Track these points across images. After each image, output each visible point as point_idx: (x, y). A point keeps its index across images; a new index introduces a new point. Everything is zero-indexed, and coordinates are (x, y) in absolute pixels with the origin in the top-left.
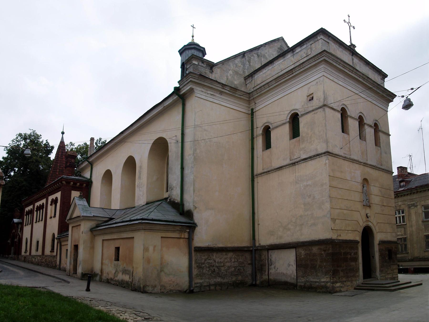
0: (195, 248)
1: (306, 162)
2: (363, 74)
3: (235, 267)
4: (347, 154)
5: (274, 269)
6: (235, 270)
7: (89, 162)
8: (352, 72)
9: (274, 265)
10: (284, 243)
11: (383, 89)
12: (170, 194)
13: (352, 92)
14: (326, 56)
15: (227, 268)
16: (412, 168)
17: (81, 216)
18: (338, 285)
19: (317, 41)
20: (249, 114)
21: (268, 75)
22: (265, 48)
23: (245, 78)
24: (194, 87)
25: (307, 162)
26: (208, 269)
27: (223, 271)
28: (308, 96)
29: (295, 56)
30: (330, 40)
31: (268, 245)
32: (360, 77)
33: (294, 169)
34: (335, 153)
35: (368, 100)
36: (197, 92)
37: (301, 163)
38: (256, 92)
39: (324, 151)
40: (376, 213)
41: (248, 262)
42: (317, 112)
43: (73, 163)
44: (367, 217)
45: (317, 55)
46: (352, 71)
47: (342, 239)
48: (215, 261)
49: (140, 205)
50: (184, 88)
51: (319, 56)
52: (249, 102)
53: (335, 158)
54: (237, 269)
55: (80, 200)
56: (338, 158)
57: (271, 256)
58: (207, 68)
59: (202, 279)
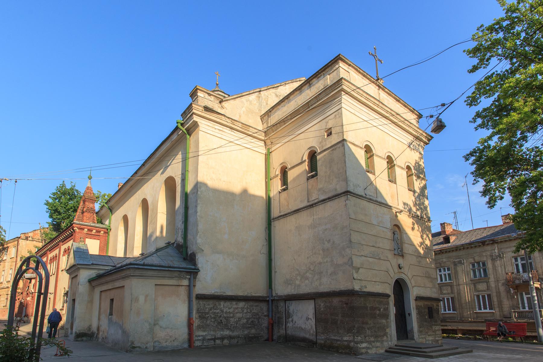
1: (324, 203)
3: (248, 318)
6: (247, 322)
9: (291, 318)
16: (457, 226)
18: (364, 345)
26: (213, 320)
36: (202, 126)
37: (319, 205)
39: (344, 190)
41: (263, 313)
48: (222, 311)
57: (288, 307)
59: (204, 331)
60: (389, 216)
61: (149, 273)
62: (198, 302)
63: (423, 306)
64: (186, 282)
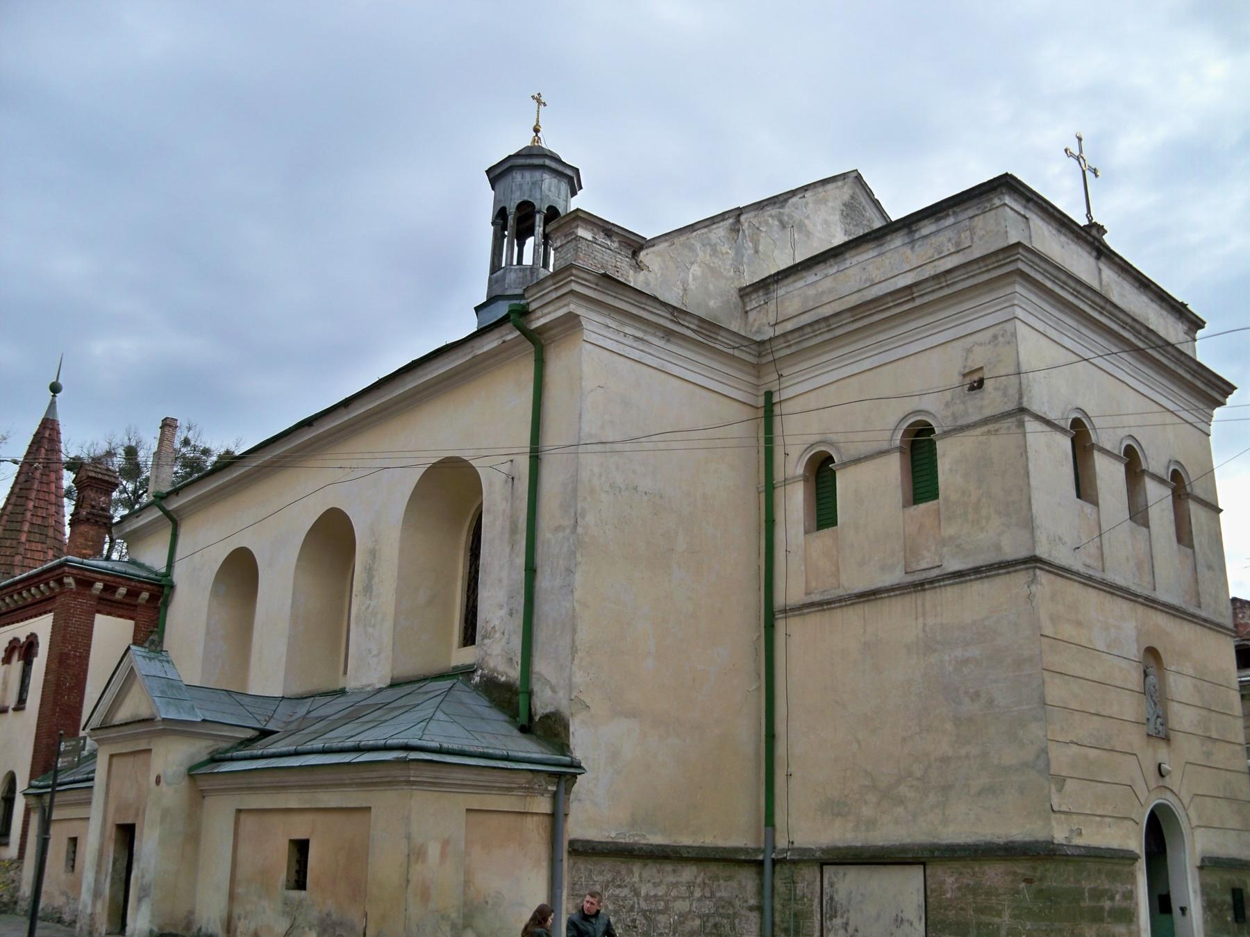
0: (572, 843)
1: (962, 582)
2: (1134, 320)
3: (704, 915)
4: (1093, 568)
5: (843, 931)
6: (704, 926)
7: (167, 514)
8: (1101, 310)
9: (842, 917)
10: (881, 844)
11: (1195, 367)
12: (483, 659)
13: (1102, 372)
14: (1022, 261)
15: (676, 917)
17: (159, 718)
19: (990, 210)
20: (758, 408)
21: (823, 293)
22: (804, 200)
23: (741, 290)
24: (579, 311)
25: (964, 585)
27: (664, 928)
28: (965, 375)
29: (917, 246)
30: (1030, 209)
31: (824, 846)
32: (1124, 328)
33: (919, 602)
34: (1057, 562)
35: (1166, 408)
36: (589, 328)
37: (945, 586)
38: (786, 342)
39: (1023, 553)
40: (1187, 763)
41: (746, 901)
42: (996, 428)
43: (103, 509)
44: (1162, 775)
45: (995, 253)
46: (1102, 308)
47: (1084, 845)
48: (637, 893)
49: (369, 686)
50: (546, 311)
51: (1001, 257)
52: (757, 369)
53: (1059, 580)
54: (710, 924)
55: (150, 659)
56: (1067, 578)
57: (832, 885)
58: (622, 253)
60: (1135, 624)
61: (454, 775)
62: (575, 863)
63: (1218, 887)
64: (543, 805)
